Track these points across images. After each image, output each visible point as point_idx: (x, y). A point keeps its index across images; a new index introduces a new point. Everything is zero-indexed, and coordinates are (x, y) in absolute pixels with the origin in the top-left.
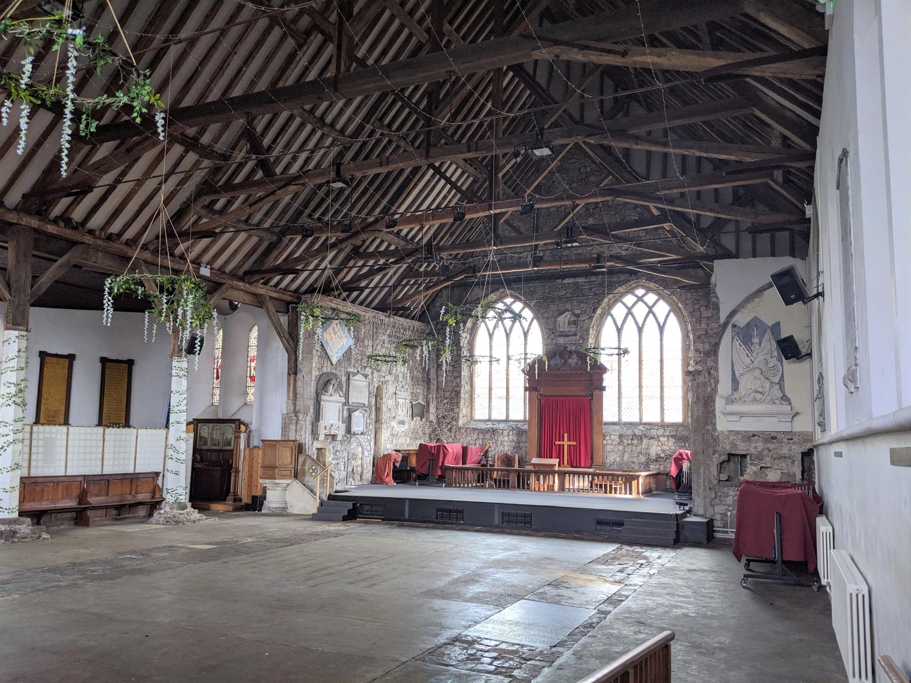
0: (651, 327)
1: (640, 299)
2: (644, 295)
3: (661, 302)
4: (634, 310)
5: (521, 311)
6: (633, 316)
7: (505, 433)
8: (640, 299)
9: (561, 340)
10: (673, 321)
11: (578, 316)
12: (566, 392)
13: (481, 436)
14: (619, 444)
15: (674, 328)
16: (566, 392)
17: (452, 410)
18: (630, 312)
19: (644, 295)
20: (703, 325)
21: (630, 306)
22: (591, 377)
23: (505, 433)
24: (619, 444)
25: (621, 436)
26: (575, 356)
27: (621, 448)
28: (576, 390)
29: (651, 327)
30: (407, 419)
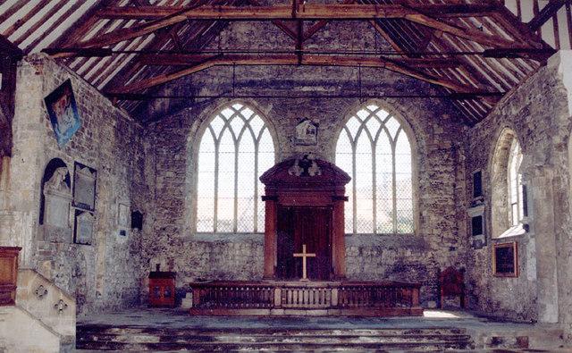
0: (383, 141)
1: (373, 114)
2: (377, 110)
3: (257, 117)
4: (251, 123)
5: (358, 118)
6: (231, 130)
7: (237, 246)
8: (237, 113)
9: (300, 149)
10: (403, 137)
11: (317, 125)
12: (304, 201)
13: (208, 250)
14: (359, 255)
15: (404, 141)
16: (304, 201)
17: (173, 222)
18: (363, 125)
19: (377, 110)
20: (436, 142)
21: (247, 118)
22: (333, 183)
23: (237, 246)
24: (359, 255)
25: (361, 249)
26: (314, 165)
27: (361, 259)
28: (315, 200)
29: (383, 141)
30: (127, 229)
